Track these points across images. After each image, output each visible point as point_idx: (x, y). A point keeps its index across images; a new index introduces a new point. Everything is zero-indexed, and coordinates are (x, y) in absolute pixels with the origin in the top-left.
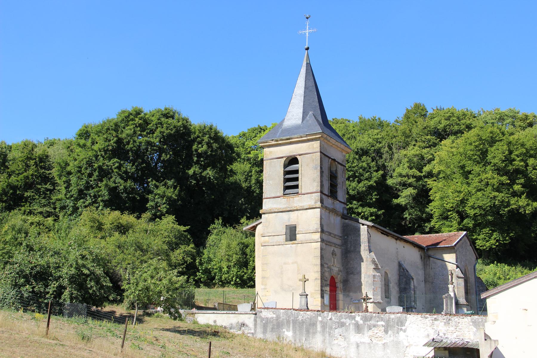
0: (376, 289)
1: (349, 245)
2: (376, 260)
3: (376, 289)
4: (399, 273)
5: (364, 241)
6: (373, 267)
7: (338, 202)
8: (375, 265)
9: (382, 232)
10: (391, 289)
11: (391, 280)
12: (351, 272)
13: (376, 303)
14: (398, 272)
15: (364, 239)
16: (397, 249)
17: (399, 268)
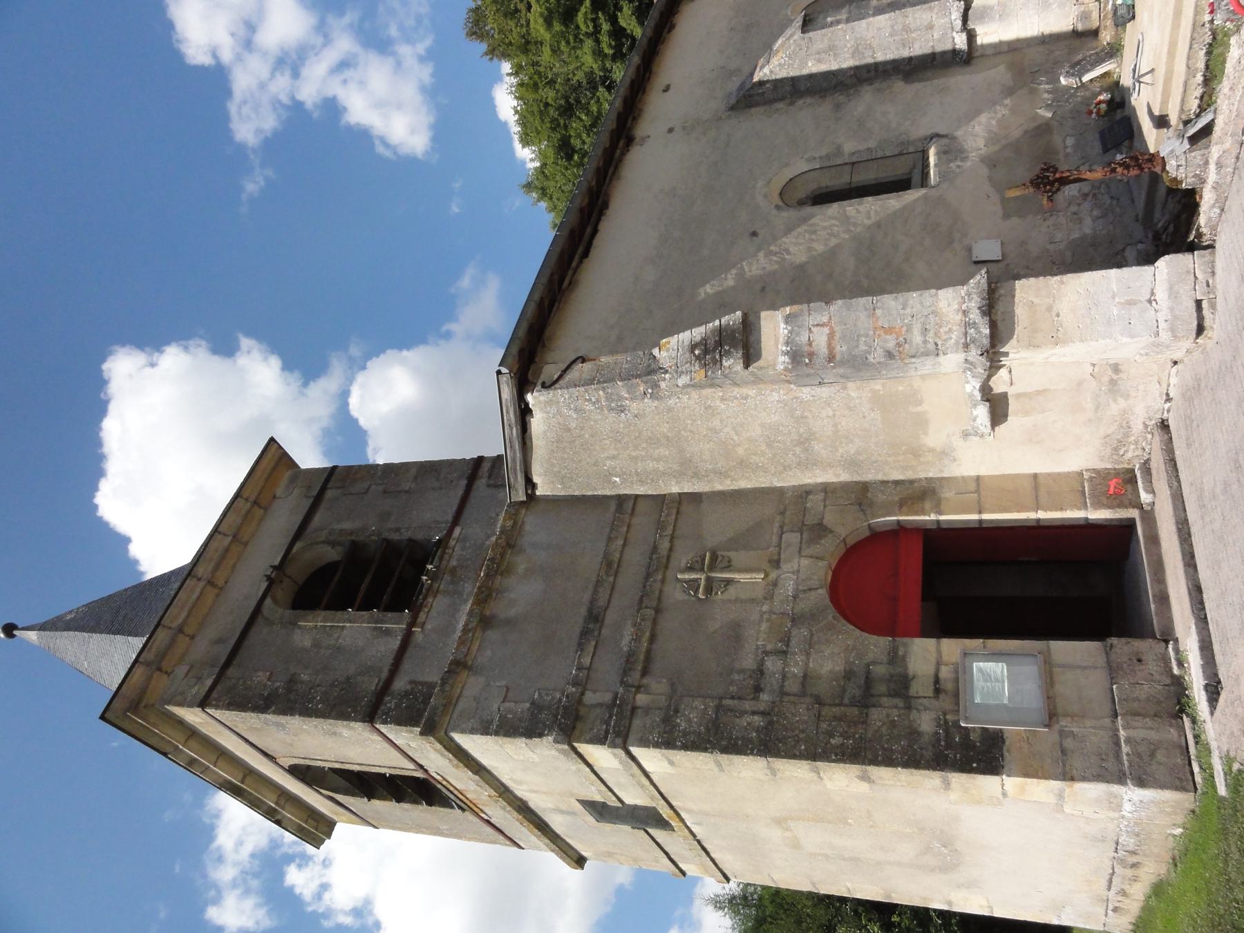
0: (889, 331)
1: (651, 465)
2: (698, 333)
3: (889, 331)
4: (782, 99)
5: (607, 399)
6: (739, 367)
7: (457, 531)
8: (728, 353)
9: (580, 250)
10: (872, 144)
11: (824, 152)
12: (798, 450)
13: (993, 325)
14: (780, 105)
15: (598, 401)
16: (671, 130)
17: (757, 105)
